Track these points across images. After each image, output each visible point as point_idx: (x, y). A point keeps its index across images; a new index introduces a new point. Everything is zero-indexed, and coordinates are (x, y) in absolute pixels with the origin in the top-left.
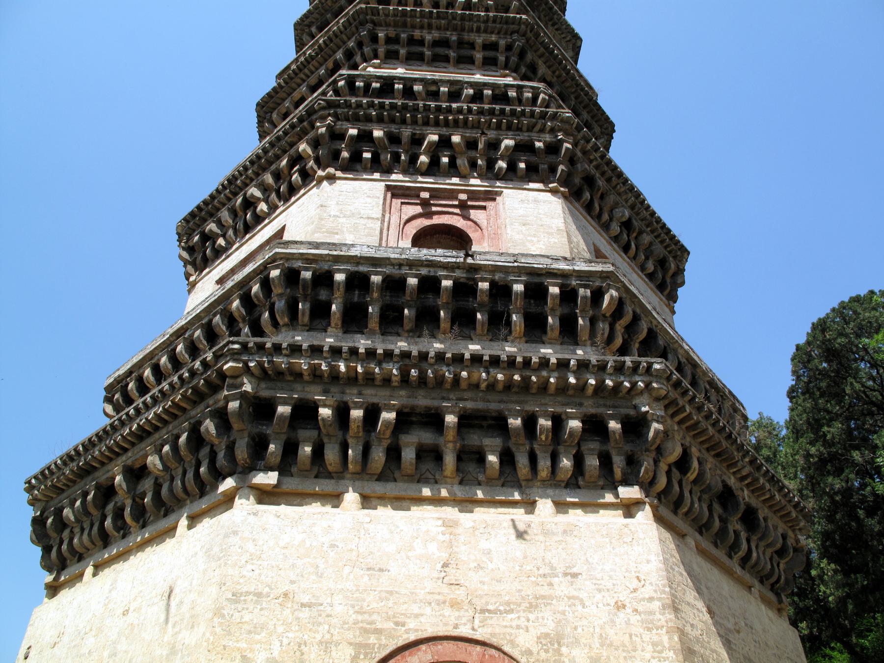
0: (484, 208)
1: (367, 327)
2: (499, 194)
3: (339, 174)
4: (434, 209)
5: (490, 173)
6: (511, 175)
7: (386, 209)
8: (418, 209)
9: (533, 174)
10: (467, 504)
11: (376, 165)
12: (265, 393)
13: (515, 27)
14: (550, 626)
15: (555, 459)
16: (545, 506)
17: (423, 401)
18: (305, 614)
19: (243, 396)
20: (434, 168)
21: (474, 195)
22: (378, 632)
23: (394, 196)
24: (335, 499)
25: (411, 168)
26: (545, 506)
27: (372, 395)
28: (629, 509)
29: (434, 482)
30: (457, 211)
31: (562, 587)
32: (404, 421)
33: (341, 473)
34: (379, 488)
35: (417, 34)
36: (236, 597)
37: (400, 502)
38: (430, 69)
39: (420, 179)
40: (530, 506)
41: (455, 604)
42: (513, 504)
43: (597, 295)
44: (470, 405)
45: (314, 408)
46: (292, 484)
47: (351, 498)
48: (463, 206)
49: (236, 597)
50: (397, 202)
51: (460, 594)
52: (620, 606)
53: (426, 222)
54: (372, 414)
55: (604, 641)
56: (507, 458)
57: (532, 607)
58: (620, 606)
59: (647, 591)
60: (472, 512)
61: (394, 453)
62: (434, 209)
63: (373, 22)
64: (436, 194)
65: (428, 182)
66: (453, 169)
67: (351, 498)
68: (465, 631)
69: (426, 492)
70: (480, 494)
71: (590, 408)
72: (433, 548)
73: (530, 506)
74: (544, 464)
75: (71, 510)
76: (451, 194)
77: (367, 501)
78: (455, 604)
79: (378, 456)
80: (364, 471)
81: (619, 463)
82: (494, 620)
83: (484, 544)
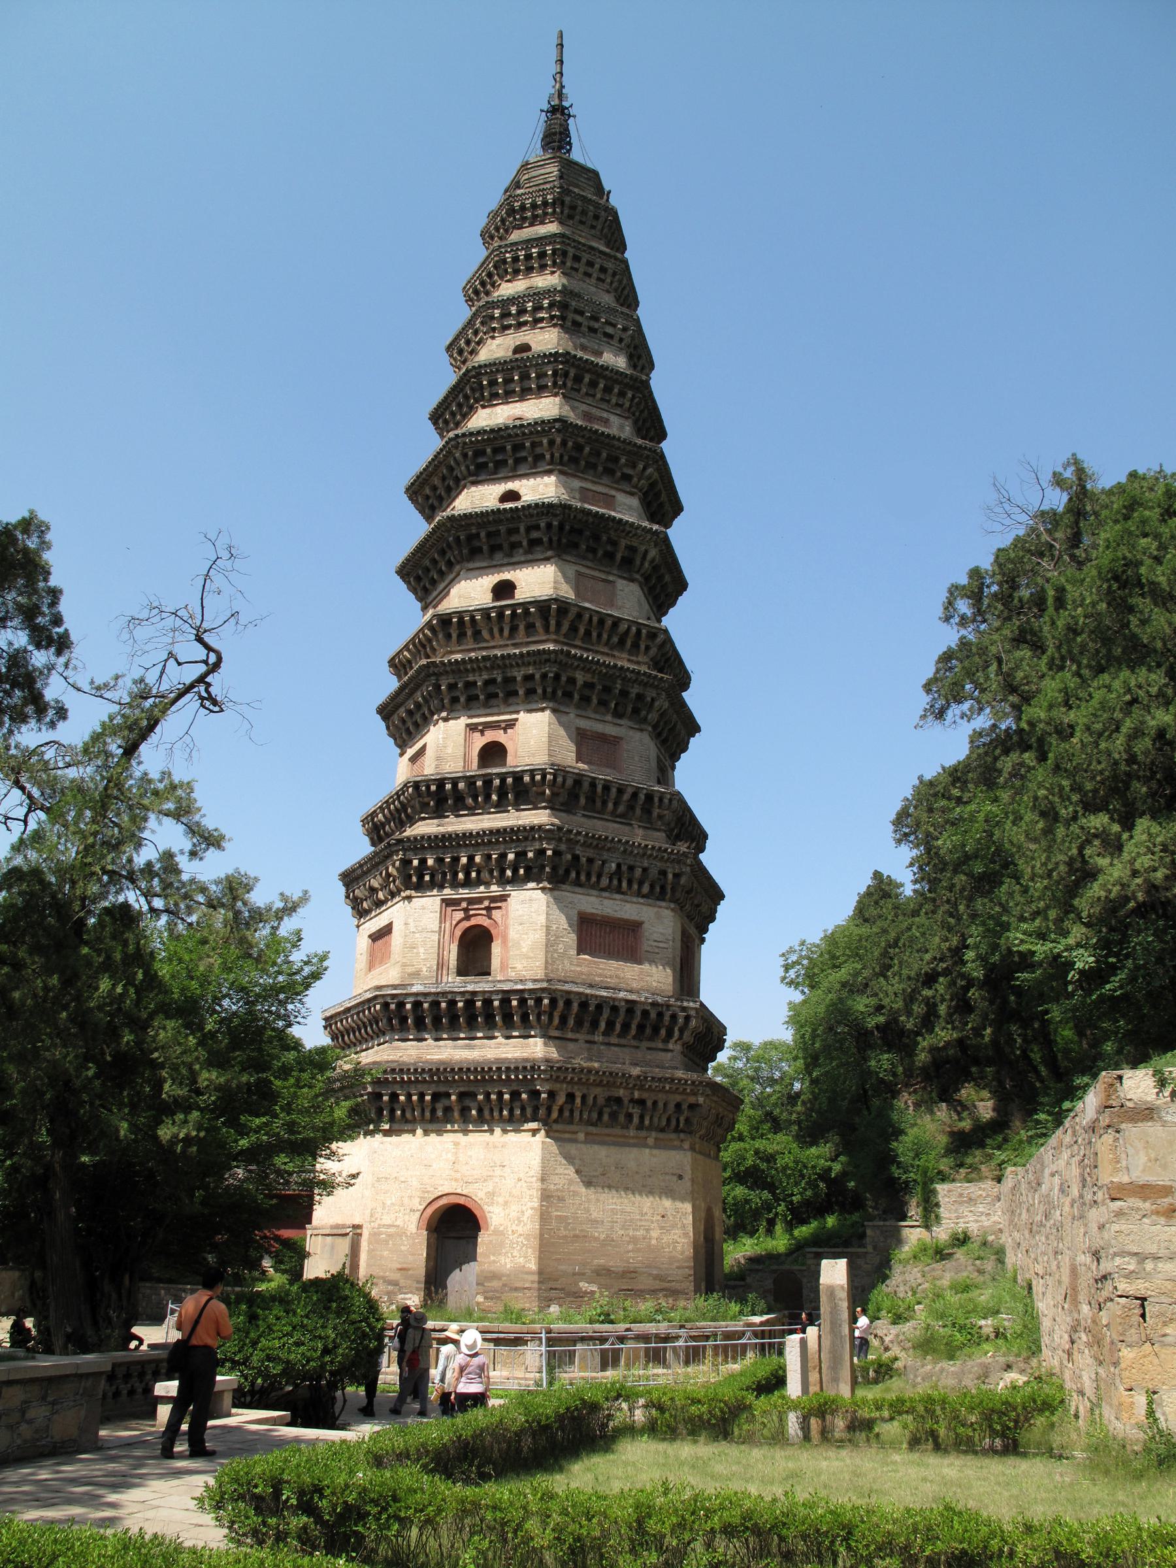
0: (499, 908)
1: (310, 1223)
2: (509, 896)
3: (413, 893)
4: (472, 912)
5: (503, 881)
6: (516, 881)
7: (443, 919)
8: (461, 915)
9: (528, 878)
10: (466, 1132)
11: (433, 884)
12: (377, 1090)
13: (546, 656)
14: (490, 1189)
15: (501, 1111)
16: (498, 1131)
17: (442, 1089)
18: (403, 1185)
19: (369, 1094)
20: (467, 883)
21: (493, 899)
22: (428, 1192)
23: (447, 905)
24: (413, 1132)
25: (455, 885)
26: (498, 1131)
27: (421, 1088)
28: (534, 1132)
29: (452, 1123)
30: (484, 912)
31: (498, 1172)
32: (436, 1097)
33: (414, 1121)
34: (430, 1127)
35: (471, 678)
36: (378, 1180)
37: (440, 1132)
38: (488, 711)
39: (461, 891)
40: (491, 1131)
41: (456, 1180)
42: (485, 1131)
43: (539, 1001)
44: (462, 1089)
45: (398, 1095)
46: (396, 1126)
47: (419, 1131)
48: (488, 909)
49: (378, 1180)
50: (449, 909)
51: (458, 1175)
52: (520, 1180)
53: (466, 924)
54: (422, 1096)
55: (511, 1194)
56: (480, 1111)
57: (485, 1180)
58: (520, 1180)
59: (532, 1173)
60: (927, 688)
61: (433, 1111)
62: (472, 912)
63: (434, 674)
64: (471, 901)
65: (464, 893)
66: (479, 882)
67: (419, 1131)
68: (459, 1191)
69: (449, 1127)
70: (471, 1127)
71: (514, 1087)
72: (450, 1155)
73: (491, 1131)
74: (496, 1114)
75: (623, 436)
76: (479, 900)
77: (426, 1133)
78: (456, 1180)
79: (428, 1114)
80: (423, 1119)
81: (529, 1111)
82: (471, 1186)
83: (469, 1153)
